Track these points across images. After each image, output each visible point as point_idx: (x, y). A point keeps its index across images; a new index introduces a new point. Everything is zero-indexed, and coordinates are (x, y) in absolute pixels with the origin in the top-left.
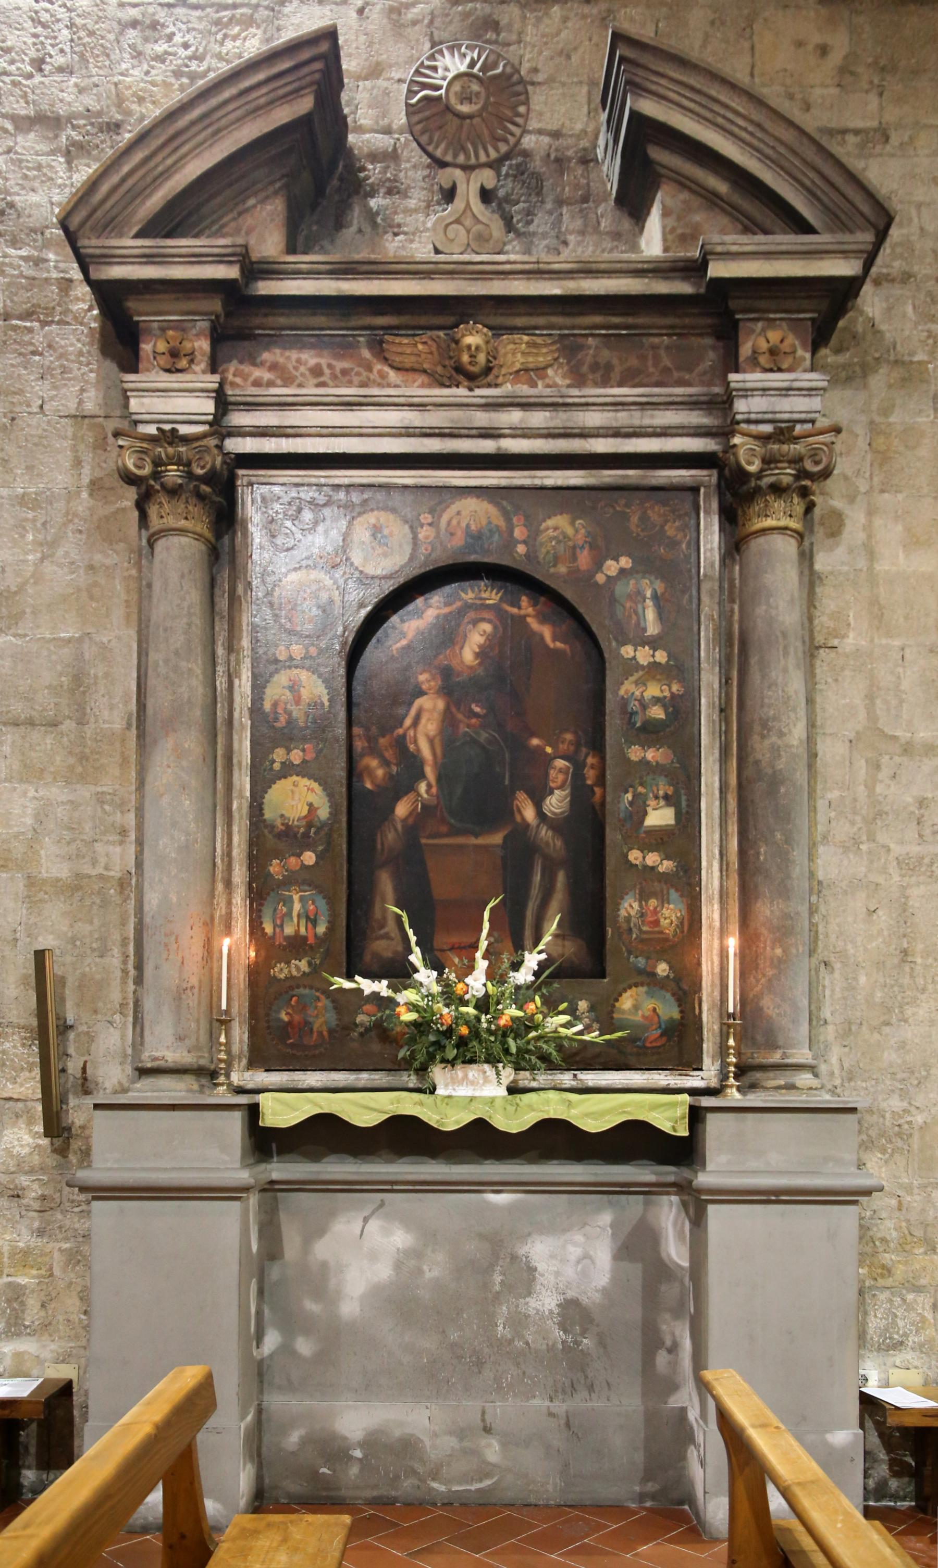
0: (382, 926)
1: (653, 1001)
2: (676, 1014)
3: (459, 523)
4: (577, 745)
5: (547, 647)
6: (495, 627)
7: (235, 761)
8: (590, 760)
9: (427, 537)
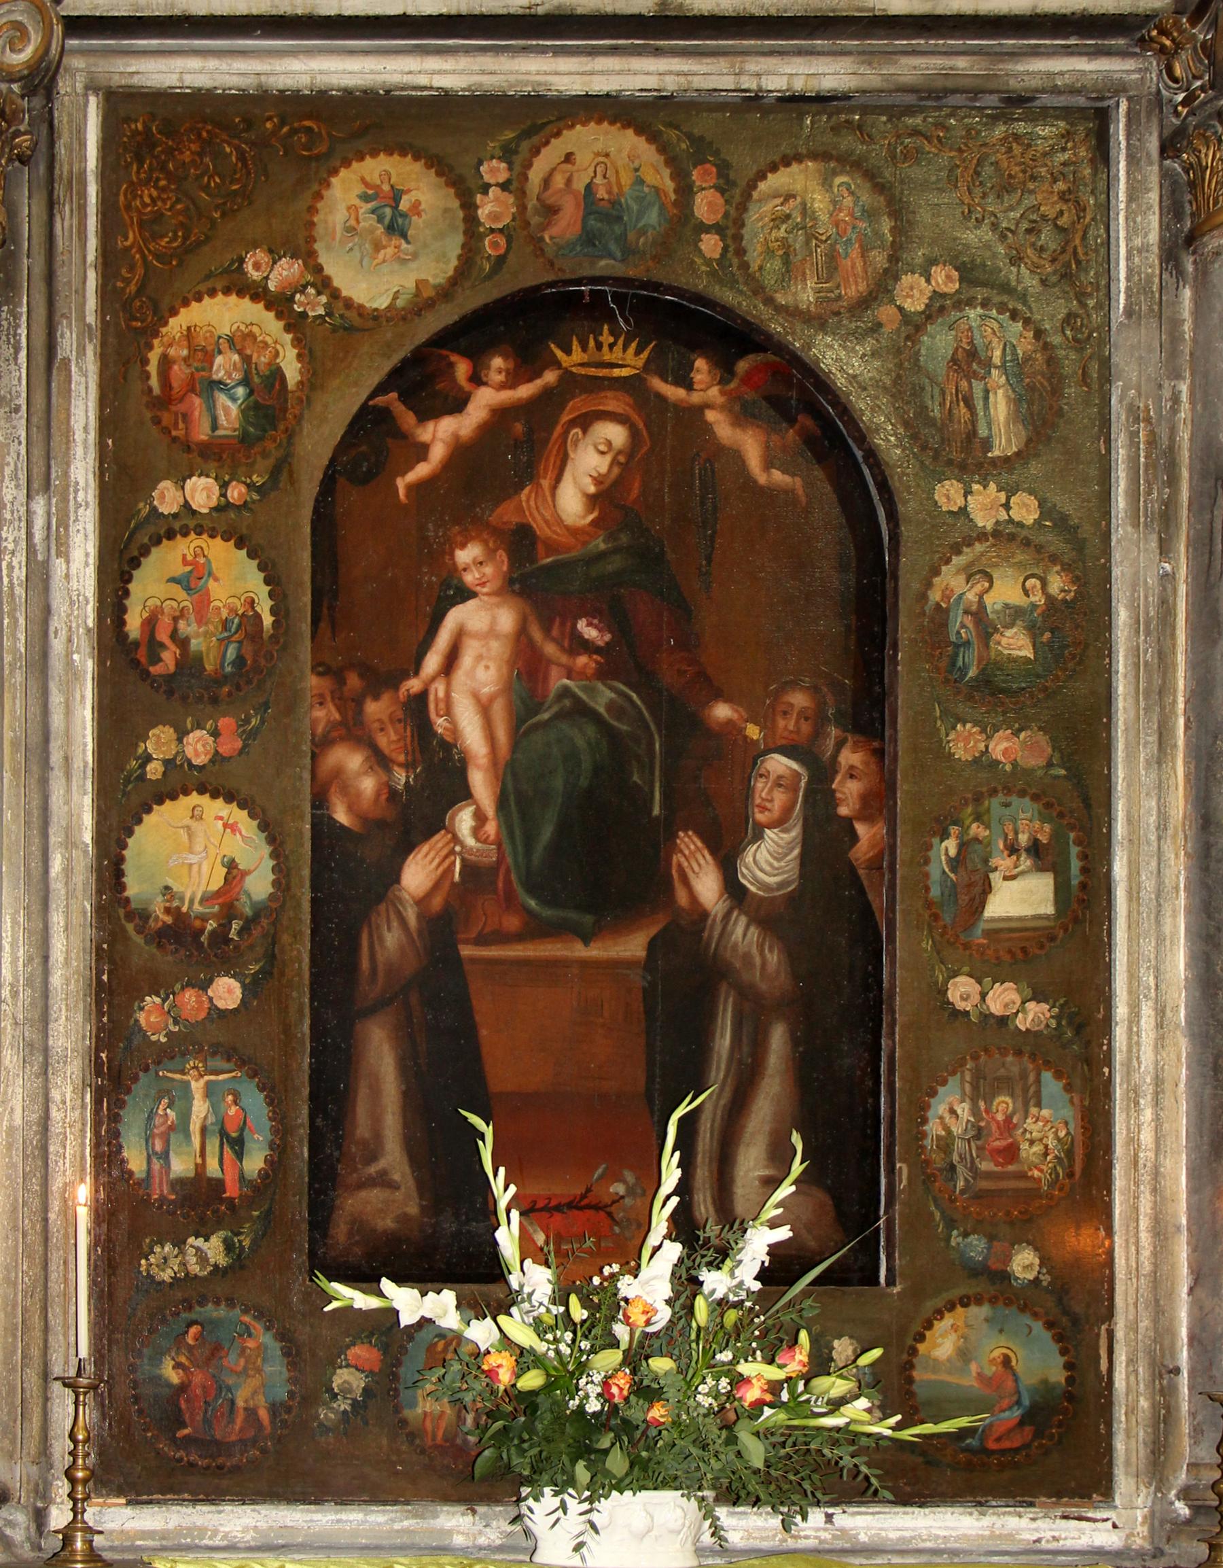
0: (373, 1157)
1: (1003, 1340)
2: (1058, 1375)
3: (569, 182)
4: (819, 720)
5: (749, 483)
6: (634, 434)
7: (56, 758)
8: (850, 757)
9: (495, 217)
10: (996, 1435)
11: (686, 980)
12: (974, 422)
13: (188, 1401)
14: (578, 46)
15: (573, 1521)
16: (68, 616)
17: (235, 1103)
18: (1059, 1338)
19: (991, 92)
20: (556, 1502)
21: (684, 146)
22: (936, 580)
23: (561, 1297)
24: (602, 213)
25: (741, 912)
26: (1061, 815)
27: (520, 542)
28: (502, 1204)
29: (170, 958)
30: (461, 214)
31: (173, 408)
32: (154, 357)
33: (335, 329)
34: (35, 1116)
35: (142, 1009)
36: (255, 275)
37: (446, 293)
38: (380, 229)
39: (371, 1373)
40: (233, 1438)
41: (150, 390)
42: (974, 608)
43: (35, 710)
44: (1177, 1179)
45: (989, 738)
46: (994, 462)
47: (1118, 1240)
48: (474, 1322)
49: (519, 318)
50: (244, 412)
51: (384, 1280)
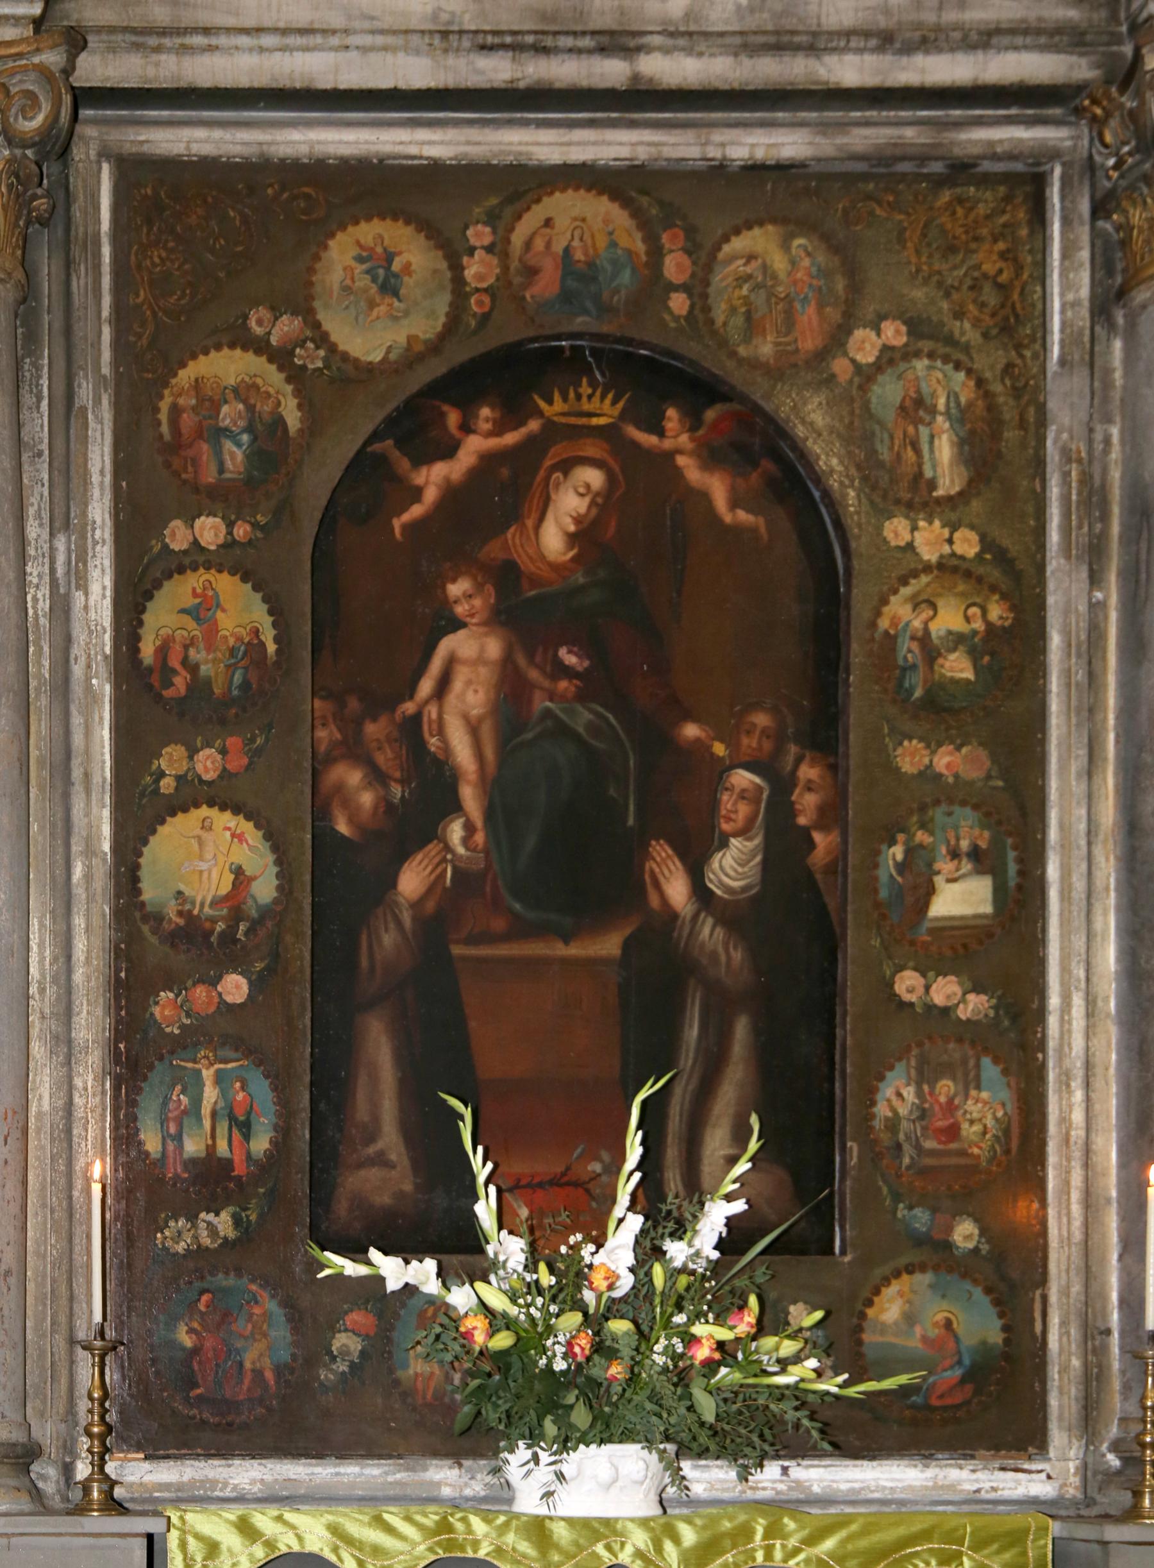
1: (945, 1305)
2: (996, 1337)
3: (548, 245)
4: (779, 738)
7: (77, 773)
8: (808, 772)
9: (480, 277)
10: (939, 1392)
11: (657, 980)
12: (920, 465)
13: (200, 1363)
14: (559, 119)
15: (543, 1474)
16: (87, 644)
17: (243, 1088)
18: (997, 1303)
19: (937, 159)
20: (528, 1454)
21: (654, 212)
22: (886, 609)
23: (531, 1266)
24: (580, 277)
25: (710, 913)
26: (999, 823)
27: (506, 577)
28: (481, 1179)
29: (183, 957)
30: (449, 275)
31: (183, 453)
32: (164, 406)
33: (332, 381)
34: (60, 1103)
35: (157, 1003)
36: (259, 331)
37: (435, 347)
38: (374, 289)
39: (367, 1337)
40: (241, 1397)
41: (161, 436)
42: (920, 634)
43: (58, 730)
44: (1108, 1155)
45: (933, 753)
46: (938, 501)
47: (1051, 1212)
48: (454, 1289)
49: (502, 369)
50: (248, 457)
51: (372, 1249)
